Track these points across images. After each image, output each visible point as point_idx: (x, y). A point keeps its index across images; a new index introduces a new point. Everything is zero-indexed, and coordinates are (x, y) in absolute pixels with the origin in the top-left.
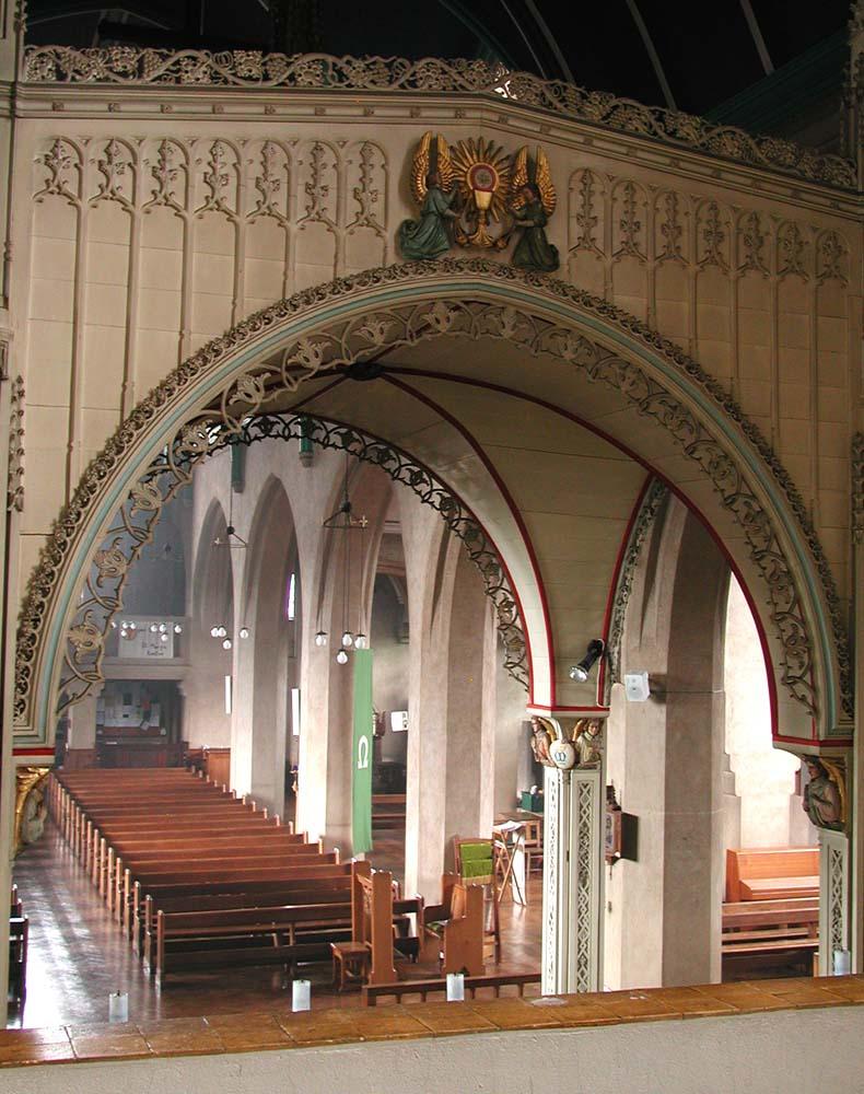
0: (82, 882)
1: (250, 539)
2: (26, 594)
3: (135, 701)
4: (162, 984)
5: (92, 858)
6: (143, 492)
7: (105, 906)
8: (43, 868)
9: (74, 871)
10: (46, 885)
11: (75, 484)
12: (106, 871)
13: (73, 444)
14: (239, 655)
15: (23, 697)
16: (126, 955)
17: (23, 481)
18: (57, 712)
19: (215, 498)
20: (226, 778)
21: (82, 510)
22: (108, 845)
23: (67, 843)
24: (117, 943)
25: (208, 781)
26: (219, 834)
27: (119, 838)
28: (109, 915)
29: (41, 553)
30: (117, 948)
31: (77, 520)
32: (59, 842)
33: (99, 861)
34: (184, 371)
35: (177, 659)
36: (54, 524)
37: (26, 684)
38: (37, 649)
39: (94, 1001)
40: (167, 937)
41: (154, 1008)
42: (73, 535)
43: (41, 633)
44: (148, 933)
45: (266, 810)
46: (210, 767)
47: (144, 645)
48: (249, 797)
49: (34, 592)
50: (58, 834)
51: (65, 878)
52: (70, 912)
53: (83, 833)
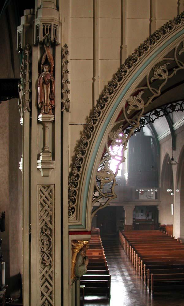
0: (129, 263)
1: (179, 161)
2: (74, 154)
3: (145, 212)
4: (153, 295)
5: (132, 256)
6: (133, 101)
7: (135, 270)
8: (117, 259)
9: (127, 259)
10: (118, 264)
11: (97, 98)
12: (136, 260)
13: (95, 78)
14: (176, 198)
15: (74, 206)
16: (142, 285)
17: (70, 96)
18: (92, 213)
19: (167, 153)
20: (172, 233)
21: (101, 111)
22: (136, 253)
23: (125, 251)
24: (139, 281)
25: (166, 234)
26: (170, 250)
27: (139, 251)
28: (137, 273)
29: (81, 133)
30: (139, 283)
31: (99, 116)
32: (122, 251)
33: (134, 257)
34: (153, 38)
35: (156, 199)
36: (87, 119)
37: (75, 199)
38: (80, 182)
39: (131, 300)
40: (154, 281)
41: (150, 303)
42: (97, 124)
43: (82, 174)
44: (148, 280)
45: (181, 241)
46: (167, 230)
47: (146, 196)
48: (179, 238)
49: (77, 153)
50: (122, 249)
51: (124, 262)
52: (125, 272)
53: (129, 249)
